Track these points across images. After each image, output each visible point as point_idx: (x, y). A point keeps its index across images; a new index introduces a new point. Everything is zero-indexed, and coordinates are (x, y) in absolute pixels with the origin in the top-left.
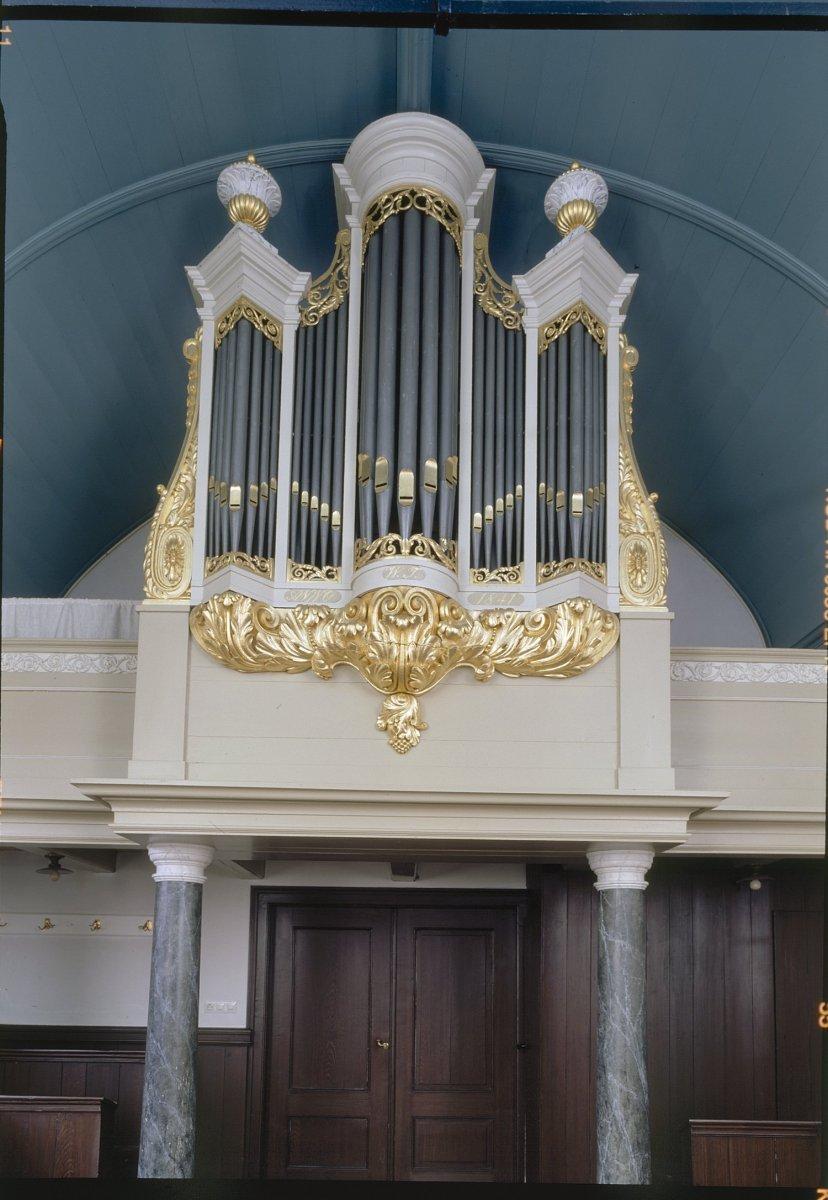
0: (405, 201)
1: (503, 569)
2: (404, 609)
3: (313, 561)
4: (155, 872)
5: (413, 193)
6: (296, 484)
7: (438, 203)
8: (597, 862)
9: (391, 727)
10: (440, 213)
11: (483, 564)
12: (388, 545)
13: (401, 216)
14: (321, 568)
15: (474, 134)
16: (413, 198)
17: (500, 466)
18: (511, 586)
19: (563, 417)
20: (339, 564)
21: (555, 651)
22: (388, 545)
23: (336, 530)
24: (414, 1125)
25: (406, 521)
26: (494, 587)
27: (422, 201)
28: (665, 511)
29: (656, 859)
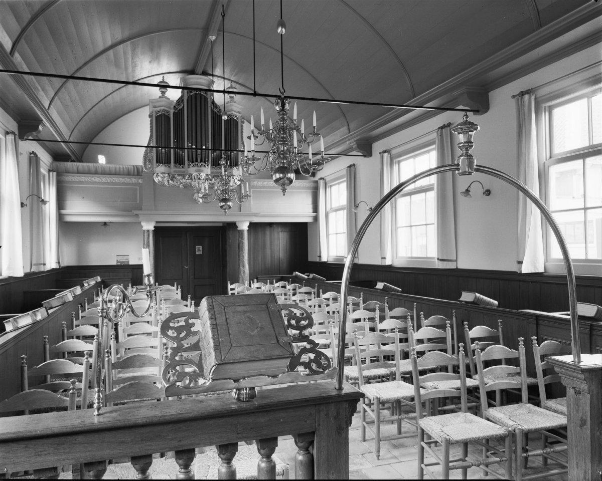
23: (183, 157)
25: (199, 160)
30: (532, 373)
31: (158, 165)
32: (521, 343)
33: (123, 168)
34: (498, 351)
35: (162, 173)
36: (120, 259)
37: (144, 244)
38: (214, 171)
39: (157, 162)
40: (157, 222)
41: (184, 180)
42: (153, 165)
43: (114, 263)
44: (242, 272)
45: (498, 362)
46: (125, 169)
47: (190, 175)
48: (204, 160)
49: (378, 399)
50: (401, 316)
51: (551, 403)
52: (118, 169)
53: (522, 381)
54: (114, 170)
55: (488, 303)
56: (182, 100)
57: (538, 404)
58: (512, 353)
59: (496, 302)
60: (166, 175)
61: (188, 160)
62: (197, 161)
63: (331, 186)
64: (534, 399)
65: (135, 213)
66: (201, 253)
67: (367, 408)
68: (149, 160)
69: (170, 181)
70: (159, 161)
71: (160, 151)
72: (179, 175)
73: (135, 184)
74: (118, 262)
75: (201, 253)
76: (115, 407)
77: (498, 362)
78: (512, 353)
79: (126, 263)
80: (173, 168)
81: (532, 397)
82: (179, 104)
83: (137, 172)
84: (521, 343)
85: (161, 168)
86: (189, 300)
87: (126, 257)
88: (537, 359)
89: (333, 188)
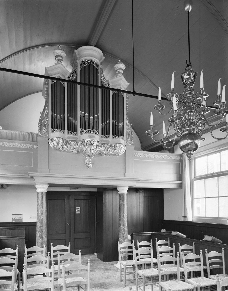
0: (90, 63)
1: (106, 136)
2: (92, 143)
3: (72, 131)
4: (37, 190)
5: (92, 61)
6: (76, 123)
7: (96, 64)
8: (118, 189)
9: (87, 164)
10: (96, 66)
11: (102, 135)
12: (89, 131)
13: (89, 65)
14: (74, 133)
15: (103, 53)
16: (92, 62)
17: (105, 116)
18: (108, 139)
19: (117, 108)
20: (77, 132)
21: (116, 152)
22: (89, 131)
23: (76, 125)
24: (75, 240)
25: (91, 127)
26: (105, 139)
27: (93, 63)
28: (133, 127)
29: (129, 188)
30: (205, 264)
31: (52, 130)
32: (174, 245)
33: (19, 134)
34: (192, 256)
35: (57, 138)
36: (14, 217)
37: (38, 205)
38: (103, 139)
39: (52, 127)
40: (51, 185)
41: (77, 146)
42: (48, 130)
43: (10, 221)
44: (123, 230)
45: (192, 260)
46: (21, 135)
47: (83, 141)
48: (95, 127)
49: (144, 276)
50: (165, 244)
51: (212, 276)
52: (14, 135)
53: (201, 268)
54: (11, 135)
55: (183, 236)
56: (76, 73)
57: (207, 277)
58: (197, 257)
59: (185, 236)
60: (61, 140)
61: (80, 128)
62: (89, 128)
63: (195, 159)
64: (206, 276)
65: (30, 175)
66: (80, 213)
67: (139, 280)
68: (45, 125)
69: (64, 146)
70: (54, 126)
71: (55, 117)
72: (72, 141)
73: (31, 150)
74: (13, 220)
75: (80, 213)
76: (44, 253)
77: (192, 260)
78: (197, 257)
79: (20, 221)
80: (66, 135)
81: (200, 273)
82: (73, 76)
83: (33, 138)
84: (174, 245)
85: (57, 133)
86: (80, 254)
87: (20, 216)
88: (207, 259)
89: (197, 160)
